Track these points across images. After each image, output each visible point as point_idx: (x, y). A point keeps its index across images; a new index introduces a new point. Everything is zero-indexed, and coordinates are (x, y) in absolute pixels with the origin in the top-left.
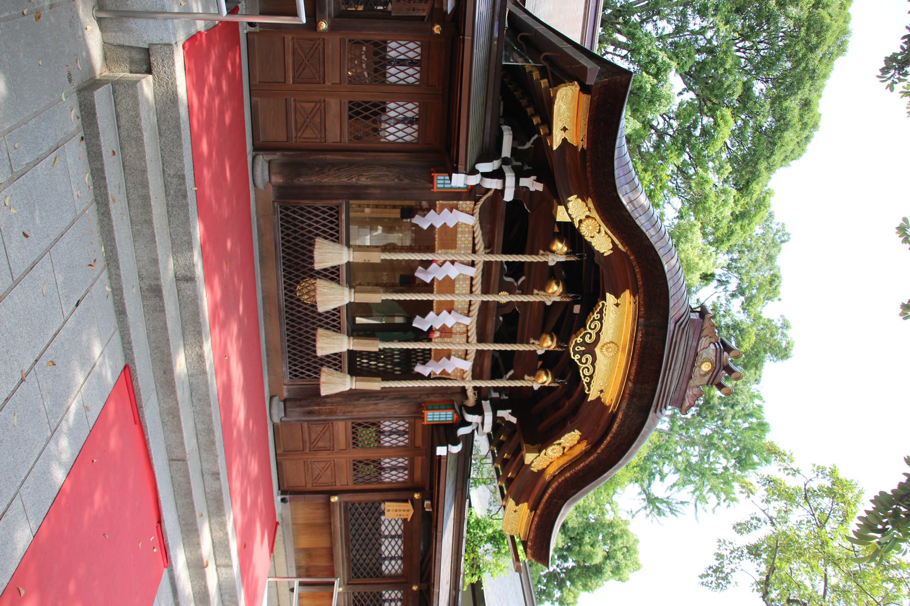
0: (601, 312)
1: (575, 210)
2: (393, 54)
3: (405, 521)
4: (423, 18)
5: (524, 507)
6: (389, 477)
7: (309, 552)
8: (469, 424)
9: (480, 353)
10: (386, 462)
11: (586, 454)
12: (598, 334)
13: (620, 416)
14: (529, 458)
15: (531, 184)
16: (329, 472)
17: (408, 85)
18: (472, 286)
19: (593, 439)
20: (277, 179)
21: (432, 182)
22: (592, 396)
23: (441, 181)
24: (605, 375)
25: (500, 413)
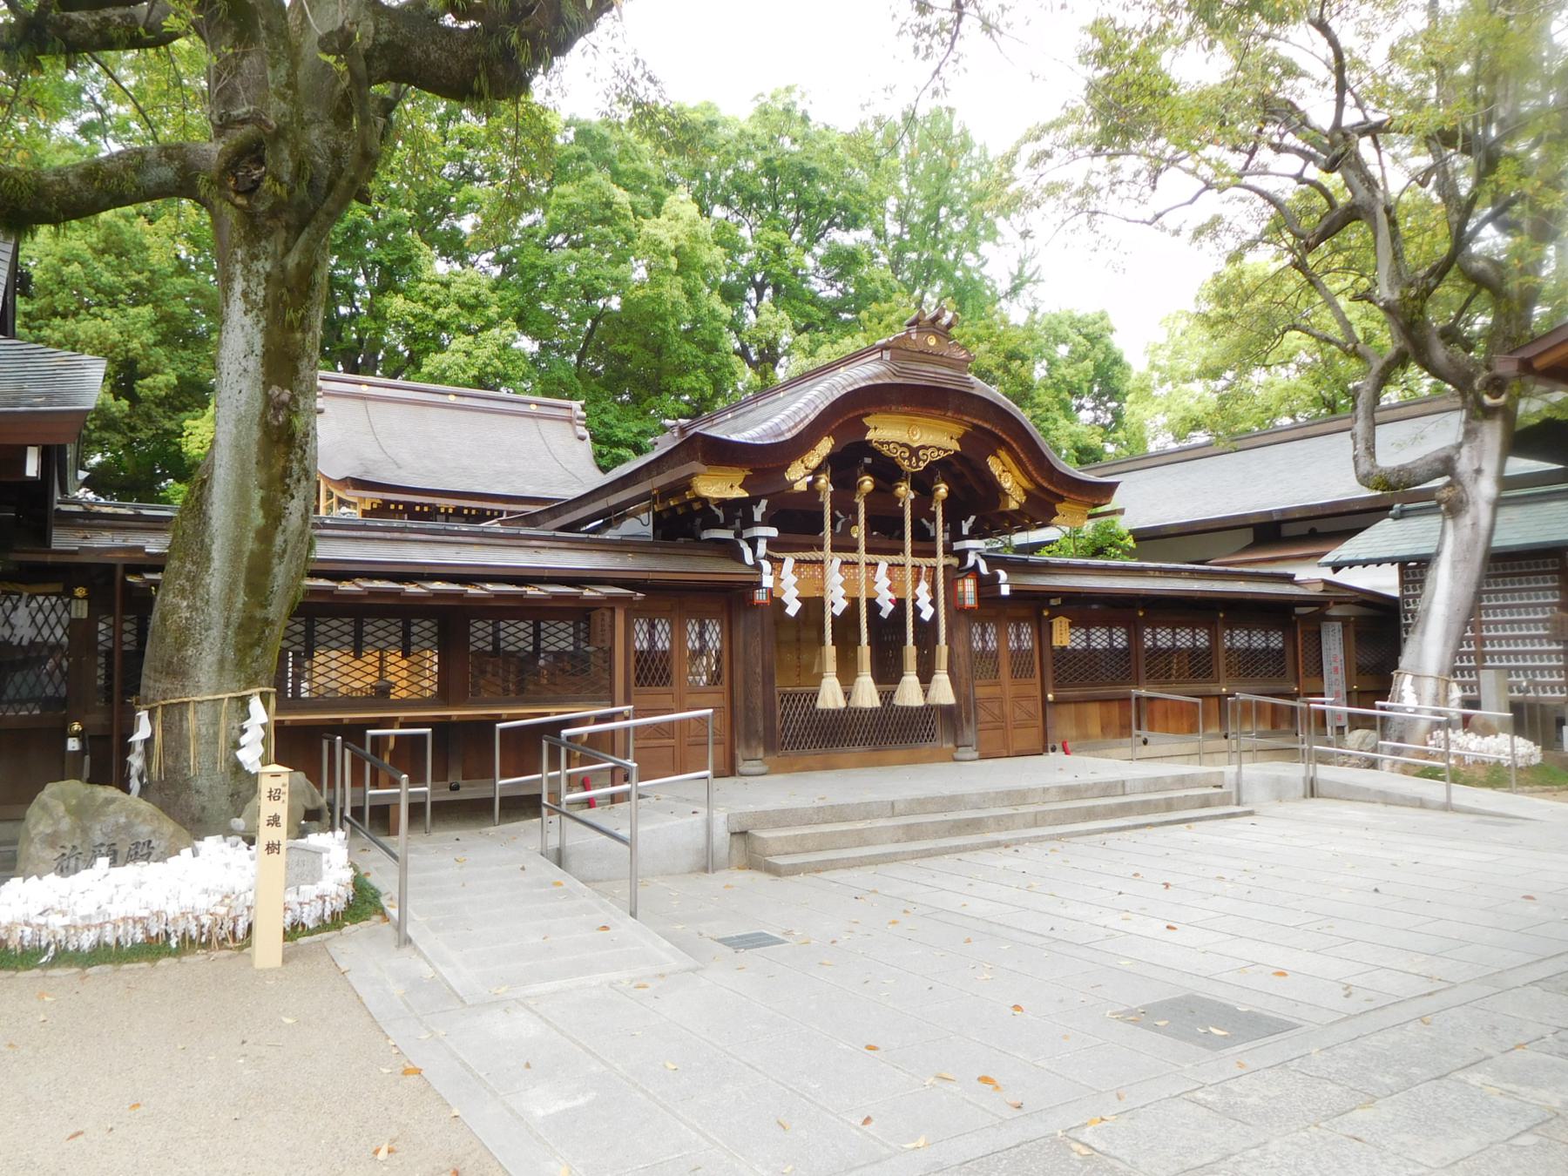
0: (882, 444)
2: (645, 645)
3: (1071, 626)
5: (1059, 507)
6: (1027, 644)
9: (915, 553)
10: (1013, 645)
11: (1010, 451)
12: (903, 445)
14: (1013, 505)
16: (1024, 703)
17: (671, 630)
18: (805, 562)
19: (993, 443)
22: (955, 446)
24: (933, 438)
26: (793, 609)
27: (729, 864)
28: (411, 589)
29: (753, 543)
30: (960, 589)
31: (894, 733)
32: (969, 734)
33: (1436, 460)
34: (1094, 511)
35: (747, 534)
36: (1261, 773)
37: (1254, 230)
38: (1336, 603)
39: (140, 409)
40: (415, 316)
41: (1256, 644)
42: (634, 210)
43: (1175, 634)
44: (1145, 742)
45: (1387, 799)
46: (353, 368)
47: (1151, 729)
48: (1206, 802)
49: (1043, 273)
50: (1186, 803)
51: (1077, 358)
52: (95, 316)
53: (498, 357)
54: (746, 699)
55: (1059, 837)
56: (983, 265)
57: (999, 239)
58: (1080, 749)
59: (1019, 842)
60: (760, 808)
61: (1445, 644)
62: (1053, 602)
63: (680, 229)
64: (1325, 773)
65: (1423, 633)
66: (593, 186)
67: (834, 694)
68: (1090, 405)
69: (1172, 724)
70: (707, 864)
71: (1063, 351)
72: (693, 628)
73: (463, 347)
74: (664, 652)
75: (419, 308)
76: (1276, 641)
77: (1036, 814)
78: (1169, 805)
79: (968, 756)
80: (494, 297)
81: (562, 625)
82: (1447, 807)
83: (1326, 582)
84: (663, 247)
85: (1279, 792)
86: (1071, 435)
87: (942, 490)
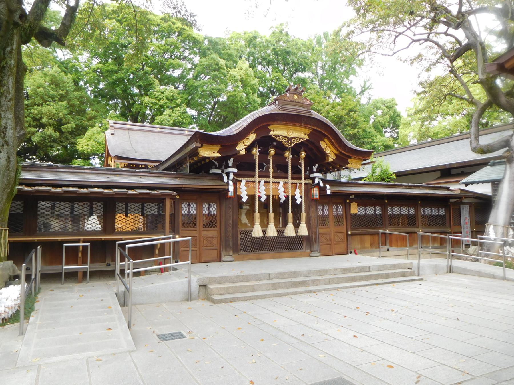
0: (276, 136)
1: (241, 148)
2: (186, 212)
3: (358, 206)
4: (174, 202)
5: (349, 161)
6: (341, 212)
7: (372, 245)
8: (319, 182)
9: (292, 178)
10: (335, 213)
11: (328, 139)
12: (284, 137)
13: (313, 128)
14: (330, 160)
15: (231, 162)
16: (339, 235)
17: (197, 207)
18: (250, 181)
19: (322, 137)
20: (231, 253)
21: (230, 198)
23: (231, 194)
24: (298, 134)
25: (314, 170)
26: (245, 199)
27: (198, 298)
28: (130, 192)
29: (228, 174)
30: (312, 192)
31: (284, 246)
32: (316, 246)
33: (503, 141)
34: (363, 162)
35: (226, 171)
36: (429, 261)
37: (434, 58)
38: (466, 198)
39: (64, 136)
40: (152, 103)
41: (436, 213)
42: (227, 67)
43: (401, 209)
44: (388, 250)
45: (480, 274)
46: (135, 120)
47: (391, 246)
48: (403, 275)
49: (373, 86)
50: (394, 275)
51: (384, 114)
52: (48, 105)
53: (180, 117)
54: (225, 233)
55: (338, 289)
56: (351, 83)
57: (356, 74)
58: (361, 253)
59: (320, 291)
60: (213, 276)
61: (507, 213)
62: (351, 197)
63: (242, 72)
64: (456, 263)
65: (497, 209)
66: (212, 58)
67: (258, 231)
68: (389, 131)
69: (399, 243)
70: (189, 297)
71: (379, 112)
72: (334, 207)
73: (168, 113)
74: (214, 215)
75: (154, 100)
76: (442, 212)
77: (329, 279)
78: (387, 276)
79: (315, 255)
80: (179, 97)
81: (153, 205)
82: (504, 278)
83: (461, 190)
84: (236, 78)
85: (436, 271)
86: (382, 141)
87: (303, 154)
